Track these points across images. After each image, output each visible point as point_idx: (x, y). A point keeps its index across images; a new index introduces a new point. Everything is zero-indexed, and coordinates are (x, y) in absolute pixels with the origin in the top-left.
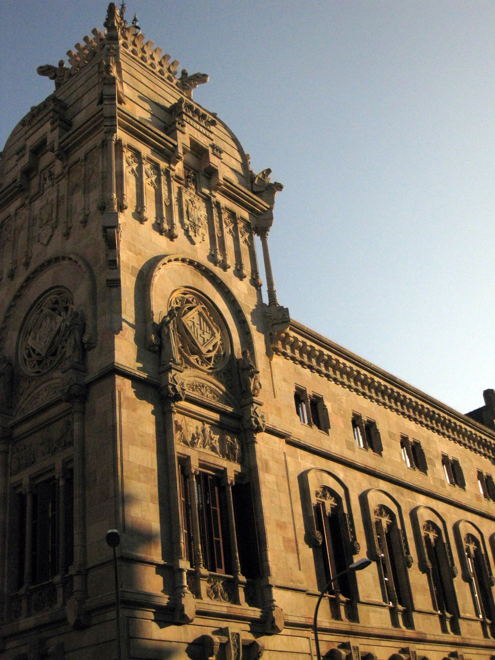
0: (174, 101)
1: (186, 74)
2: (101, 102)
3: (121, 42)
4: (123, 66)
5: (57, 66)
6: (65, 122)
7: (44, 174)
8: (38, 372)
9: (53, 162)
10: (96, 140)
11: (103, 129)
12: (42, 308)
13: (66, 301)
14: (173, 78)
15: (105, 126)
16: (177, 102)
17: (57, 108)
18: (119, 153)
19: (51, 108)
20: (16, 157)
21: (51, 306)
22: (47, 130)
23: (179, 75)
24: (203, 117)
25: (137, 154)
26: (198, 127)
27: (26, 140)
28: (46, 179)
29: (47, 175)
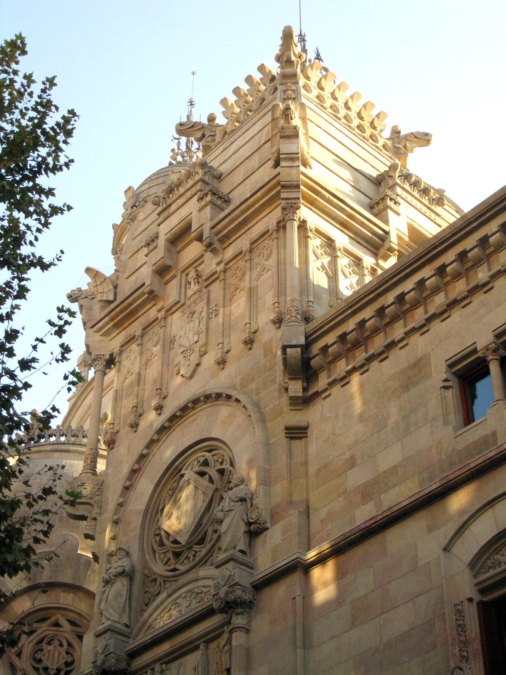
0: (383, 169)
1: (399, 133)
2: (277, 164)
3: (302, 81)
4: (309, 114)
5: (205, 121)
6: (220, 197)
7: (187, 275)
8: (175, 570)
9: (203, 256)
10: (269, 220)
11: (280, 204)
12: (183, 472)
13: (220, 460)
14: (379, 137)
15: (283, 199)
16: (387, 169)
17: (206, 178)
18: (302, 240)
19: (197, 178)
20: (145, 250)
21: (197, 468)
22: (192, 210)
23: (387, 134)
24: (425, 191)
25: (330, 243)
26: (419, 205)
27: (159, 225)
28: (190, 283)
29: (192, 274)
